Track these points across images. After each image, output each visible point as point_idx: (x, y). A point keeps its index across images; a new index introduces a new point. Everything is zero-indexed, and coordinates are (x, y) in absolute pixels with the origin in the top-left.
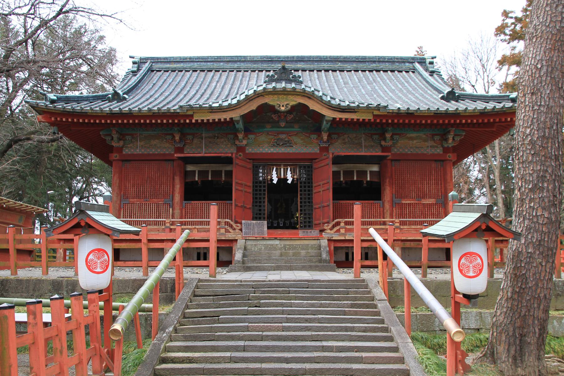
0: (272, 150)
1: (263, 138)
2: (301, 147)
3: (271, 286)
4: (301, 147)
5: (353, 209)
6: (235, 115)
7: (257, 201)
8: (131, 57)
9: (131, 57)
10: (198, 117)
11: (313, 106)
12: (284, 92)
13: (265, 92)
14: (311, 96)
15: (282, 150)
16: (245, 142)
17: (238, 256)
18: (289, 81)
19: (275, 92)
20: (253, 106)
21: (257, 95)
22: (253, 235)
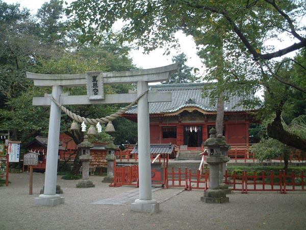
0: (190, 122)
1: (186, 118)
2: (199, 121)
3: (172, 117)
4: (199, 121)
5: (277, 185)
6: (176, 114)
7: (185, 138)
8: (164, 54)
9: (164, 54)
10: (165, 115)
11: (199, 110)
12: (190, 107)
13: (185, 107)
14: (198, 108)
15: (193, 122)
16: (181, 119)
17: (177, 156)
18: (192, 103)
19: (187, 107)
20: (182, 111)
21: (182, 108)
22: (183, 149)
